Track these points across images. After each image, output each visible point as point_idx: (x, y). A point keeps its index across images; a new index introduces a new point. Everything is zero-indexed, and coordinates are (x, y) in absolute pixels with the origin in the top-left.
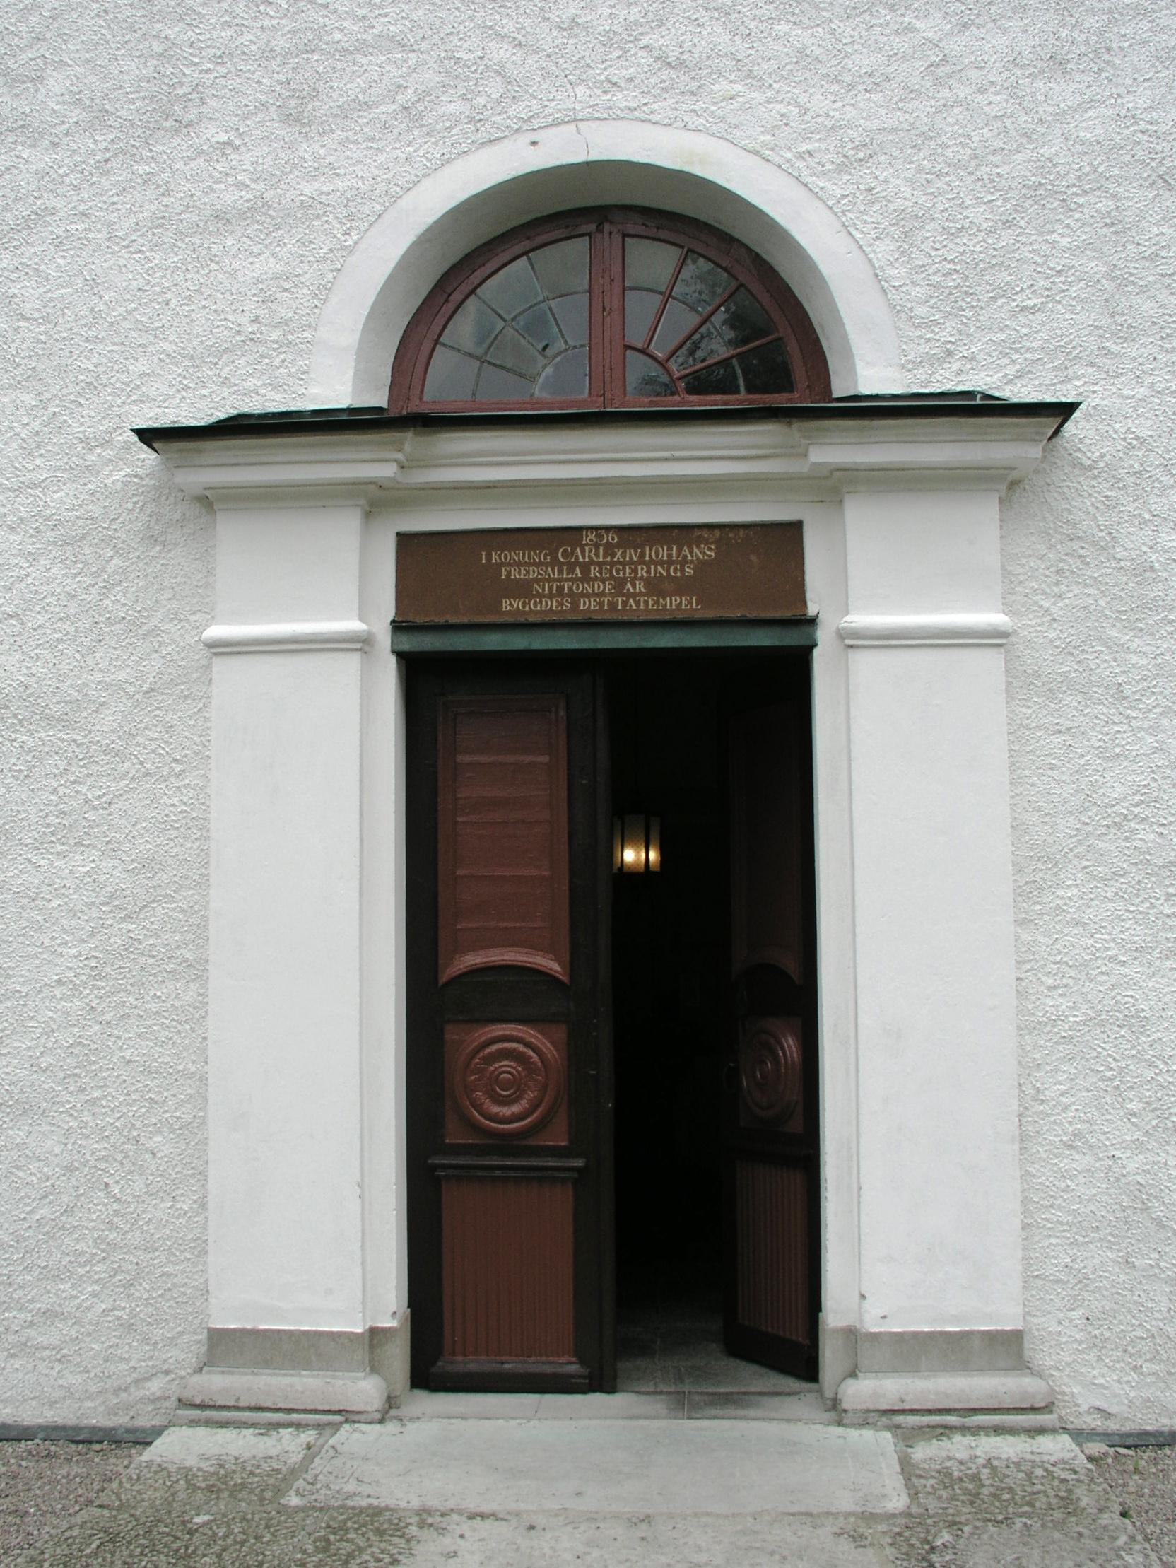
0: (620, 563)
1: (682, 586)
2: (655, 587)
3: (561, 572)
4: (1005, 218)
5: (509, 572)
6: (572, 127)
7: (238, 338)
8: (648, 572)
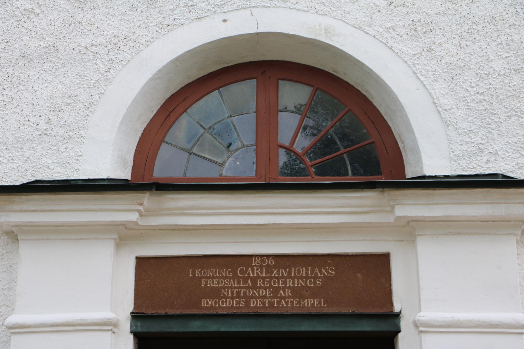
0: (276, 278)
1: (314, 293)
2: (298, 293)
3: (239, 282)
4: (516, 67)
5: (206, 283)
6: (248, 11)
7: (37, 133)
8: (294, 283)
